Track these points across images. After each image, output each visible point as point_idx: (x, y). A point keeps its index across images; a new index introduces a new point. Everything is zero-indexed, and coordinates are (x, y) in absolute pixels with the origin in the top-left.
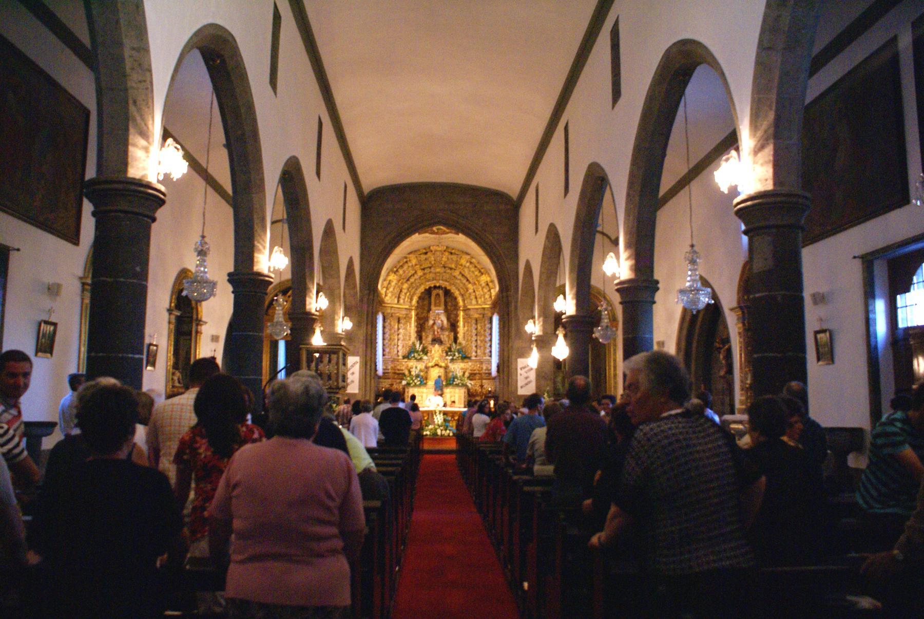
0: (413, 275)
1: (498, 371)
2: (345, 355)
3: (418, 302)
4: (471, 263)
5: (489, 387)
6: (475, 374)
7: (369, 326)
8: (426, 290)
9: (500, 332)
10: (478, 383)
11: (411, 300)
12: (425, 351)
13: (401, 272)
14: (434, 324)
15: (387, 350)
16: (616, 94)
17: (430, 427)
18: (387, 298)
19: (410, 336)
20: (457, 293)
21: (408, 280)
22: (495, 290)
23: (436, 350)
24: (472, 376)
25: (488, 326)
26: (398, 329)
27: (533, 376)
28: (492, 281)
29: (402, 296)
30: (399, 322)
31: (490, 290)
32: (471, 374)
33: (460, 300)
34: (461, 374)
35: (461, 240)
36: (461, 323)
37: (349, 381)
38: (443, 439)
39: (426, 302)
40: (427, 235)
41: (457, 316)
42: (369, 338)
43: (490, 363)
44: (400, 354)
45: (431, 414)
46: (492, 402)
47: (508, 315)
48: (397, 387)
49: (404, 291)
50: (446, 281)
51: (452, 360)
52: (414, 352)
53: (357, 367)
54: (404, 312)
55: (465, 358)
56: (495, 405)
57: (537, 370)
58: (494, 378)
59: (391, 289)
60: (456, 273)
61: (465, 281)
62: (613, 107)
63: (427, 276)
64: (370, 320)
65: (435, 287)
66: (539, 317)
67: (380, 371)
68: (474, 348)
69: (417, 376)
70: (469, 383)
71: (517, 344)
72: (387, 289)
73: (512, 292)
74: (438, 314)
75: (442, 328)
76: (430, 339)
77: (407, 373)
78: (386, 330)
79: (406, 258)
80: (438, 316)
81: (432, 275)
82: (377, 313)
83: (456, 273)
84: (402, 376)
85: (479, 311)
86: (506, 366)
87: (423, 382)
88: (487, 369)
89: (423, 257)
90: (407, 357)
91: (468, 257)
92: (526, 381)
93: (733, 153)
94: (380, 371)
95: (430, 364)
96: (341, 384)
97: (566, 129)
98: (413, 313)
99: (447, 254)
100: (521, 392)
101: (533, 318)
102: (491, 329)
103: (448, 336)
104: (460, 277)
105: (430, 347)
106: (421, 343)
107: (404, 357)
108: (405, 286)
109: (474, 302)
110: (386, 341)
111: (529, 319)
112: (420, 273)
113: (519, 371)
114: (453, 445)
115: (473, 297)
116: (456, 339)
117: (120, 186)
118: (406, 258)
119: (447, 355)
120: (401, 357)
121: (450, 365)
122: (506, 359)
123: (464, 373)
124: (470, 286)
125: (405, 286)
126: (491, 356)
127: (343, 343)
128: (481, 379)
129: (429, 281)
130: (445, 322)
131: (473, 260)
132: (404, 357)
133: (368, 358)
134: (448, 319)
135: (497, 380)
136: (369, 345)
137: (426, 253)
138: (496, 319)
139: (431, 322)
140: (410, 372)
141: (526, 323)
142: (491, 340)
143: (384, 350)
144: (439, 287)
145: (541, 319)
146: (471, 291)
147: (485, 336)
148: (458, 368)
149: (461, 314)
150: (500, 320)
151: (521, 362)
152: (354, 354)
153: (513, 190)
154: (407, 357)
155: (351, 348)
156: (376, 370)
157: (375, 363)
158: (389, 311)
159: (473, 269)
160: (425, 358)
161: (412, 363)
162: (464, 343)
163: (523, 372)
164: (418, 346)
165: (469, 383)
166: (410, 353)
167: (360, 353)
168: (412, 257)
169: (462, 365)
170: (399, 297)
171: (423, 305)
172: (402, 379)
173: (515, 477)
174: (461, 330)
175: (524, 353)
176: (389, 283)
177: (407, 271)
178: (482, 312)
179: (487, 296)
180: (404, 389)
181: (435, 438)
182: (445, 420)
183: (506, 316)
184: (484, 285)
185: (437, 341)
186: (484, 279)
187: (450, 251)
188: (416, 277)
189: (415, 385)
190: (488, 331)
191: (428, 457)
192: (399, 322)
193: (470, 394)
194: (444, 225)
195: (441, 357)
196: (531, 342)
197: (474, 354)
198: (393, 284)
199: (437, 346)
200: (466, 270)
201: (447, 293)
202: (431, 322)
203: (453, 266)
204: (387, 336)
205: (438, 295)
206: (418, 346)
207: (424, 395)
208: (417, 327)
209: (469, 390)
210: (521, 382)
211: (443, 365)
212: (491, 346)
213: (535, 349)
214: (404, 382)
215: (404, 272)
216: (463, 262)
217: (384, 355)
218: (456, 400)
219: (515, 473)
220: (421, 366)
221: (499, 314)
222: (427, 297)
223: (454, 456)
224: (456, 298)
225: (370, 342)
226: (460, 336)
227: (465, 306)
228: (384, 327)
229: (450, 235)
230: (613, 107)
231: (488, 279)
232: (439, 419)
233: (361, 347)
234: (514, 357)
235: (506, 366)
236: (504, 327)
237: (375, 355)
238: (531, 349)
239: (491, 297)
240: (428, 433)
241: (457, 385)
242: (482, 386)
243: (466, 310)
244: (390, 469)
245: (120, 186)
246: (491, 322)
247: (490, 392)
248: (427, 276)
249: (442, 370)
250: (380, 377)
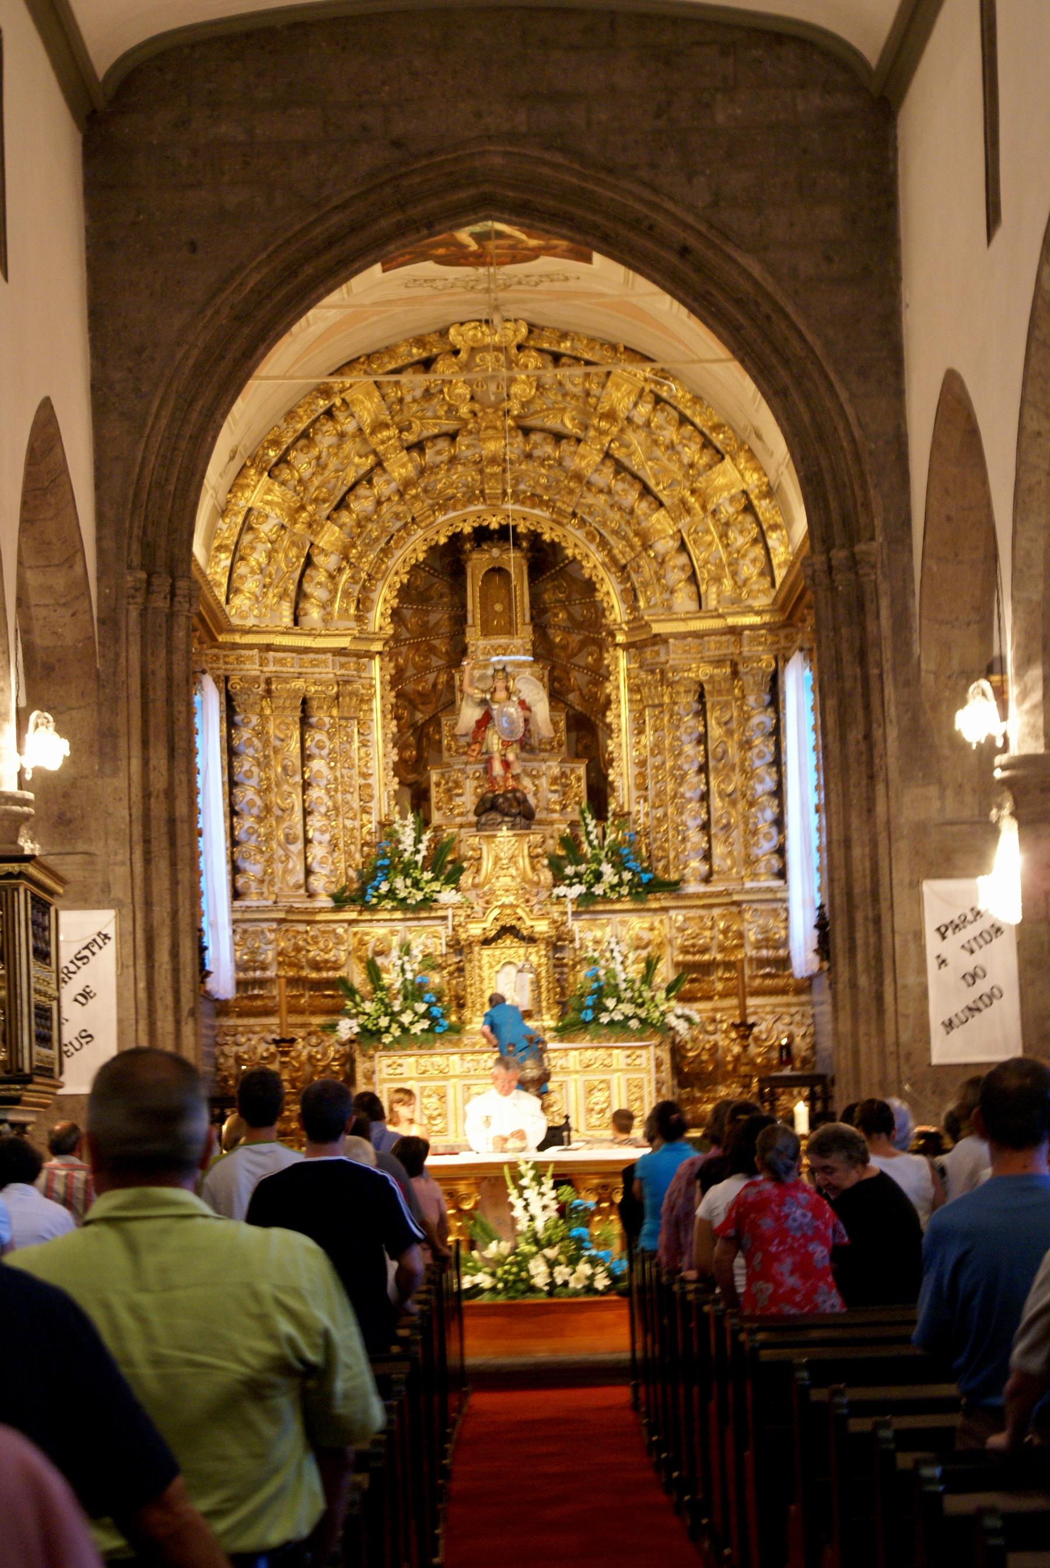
0: (367, 478)
1: (824, 947)
2: (41, 906)
3: (396, 615)
5: (777, 1024)
6: (707, 968)
7: (159, 756)
8: (433, 549)
9: (825, 750)
10: (727, 1011)
11: (363, 604)
12: (445, 863)
13: (303, 463)
14: (486, 721)
15: (253, 869)
17: (493, 1249)
18: (239, 601)
19: (366, 797)
20: (593, 562)
21: (342, 504)
22: (793, 529)
23: (504, 860)
24: (692, 979)
25: (763, 719)
26: (306, 757)
27: (1002, 963)
28: (770, 492)
29: (317, 591)
30: (305, 723)
31: (761, 538)
32: (684, 969)
33: (610, 591)
34: (635, 971)
35: (604, 290)
36: (621, 715)
37: (69, 1033)
38: (559, 1306)
39: (439, 616)
40: (428, 268)
41: (600, 675)
42: (158, 808)
43: (778, 906)
44: (318, 883)
45: (493, 1181)
46: (801, 1111)
47: (862, 657)
48: (316, 1050)
49: (326, 562)
50: (535, 500)
51: (587, 900)
52: (388, 871)
53: (107, 958)
54: (329, 670)
55: (651, 886)
56: (814, 1121)
57: (1020, 927)
58: (805, 986)
59: (257, 557)
60: (587, 459)
61: (630, 497)
63: (441, 481)
64: (158, 720)
65: (482, 535)
66: (1024, 664)
67: (223, 982)
68: (696, 838)
69: (414, 992)
70: (677, 1015)
71: (913, 805)
72: (238, 555)
73: (874, 548)
74: (503, 671)
75: (526, 744)
76: (467, 800)
77: (358, 978)
78: (245, 765)
79: (325, 392)
80: (505, 681)
81: (463, 475)
82: (192, 680)
83: (587, 459)
84: (332, 994)
85: (712, 648)
86: (861, 923)
87: (442, 1027)
88: (767, 942)
89: (414, 382)
90: (354, 897)
91: (646, 371)
92: (970, 996)
93: (883, 1136)
94: (223, 982)
95: (475, 930)
96: (31, 1054)
98: (376, 671)
99: (532, 360)
100: (947, 1049)
101: (992, 668)
102: (777, 733)
103: (561, 781)
104: (605, 477)
105: (470, 841)
106: (424, 823)
107: (340, 901)
108: (330, 536)
109: (683, 600)
110: (247, 822)
111: (970, 677)
112: (401, 467)
113: (933, 945)
114: (611, 1338)
115: (676, 576)
116: (599, 795)
118: (325, 392)
119: (559, 878)
120: (324, 901)
121: (575, 926)
122: (861, 886)
123: (651, 965)
124: (659, 521)
125: (330, 536)
126: (782, 874)
127: (28, 847)
128: (741, 992)
129: (445, 503)
130: (542, 709)
131: (671, 389)
132: (340, 901)
133: (161, 912)
134: (556, 697)
135: (822, 995)
136: (161, 844)
138: (798, 684)
139: (469, 715)
140: (374, 972)
141: (961, 701)
142: (779, 793)
143: (235, 870)
144: (504, 534)
145: (1036, 673)
146: (665, 545)
147: (749, 774)
148: (618, 939)
149: (621, 664)
150: (822, 689)
151: (940, 899)
152: (85, 901)
154: (354, 897)
155: (69, 867)
156: (203, 973)
157: (198, 933)
158: (252, 669)
159: (670, 434)
160: (448, 896)
161: (382, 929)
162: (640, 810)
163: (951, 946)
164: (407, 838)
165: (677, 1015)
166: (368, 878)
167: (120, 891)
168: (357, 382)
169: (637, 925)
170: (301, 595)
171: (425, 630)
172: (339, 1011)
173: (957, 1504)
174: (625, 747)
175: (960, 850)
176: (247, 527)
177: (335, 459)
178: (728, 648)
179: (749, 570)
180: (348, 1060)
181: (522, 1304)
182: (563, 1211)
183: (851, 669)
184: (728, 510)
185: (503, 807)
186: (729, 479)
187: (549, 346)
188: (382, 486)
189: (406, 1039)
190: (763, 747)
191: (482, 1401)
192: (305, 723)
193: (686, 1070)
194: (522, 212)
195: (527, 888)
196: (987, 791)
197: (696, 864)
198: (266, 529)
199: (504, 833)
200: (635, 439)
201: (544, 559)
202: (469, 715)
203: (569, 426)
204: (247, 794)
205: (498, 571)
206: (407, 838)
207: (453, 1089)
208: (398, 742)
209: (677, 1051)
210: (944, 996)
211: (542, 927)
212: (779, 822)
213: (1009, 830)
214: (347, 1027)
215: (320, 466)
216: (619, 397)
217: (236, 894)
218: (607, 1087)
219: (955, 1484)
220: (428, 938)
221: (808, 654)
222: (440, 586)
223: (620, 1394)
224: (590, 587)
225: (167, 834)
226: (622, 776)
227: (637, 623)
228: (231, 752)
229: (545, 264)
231: (752, 479)
232: (535, 1207)
233: (117, 859)
234: (901, 873)
235: (861, 923)
236: (843, 724)
237: (196, 895)
238: (994, 830)
239: (768, 570)
240: (484, 1280)
241: (619, 1027)
242: (744, 1028)
243: (644, 643)
246: (775, 701)
247: (786, 1051)
248: (441, 481)
249: (537, 955)
250: (222, 1008)
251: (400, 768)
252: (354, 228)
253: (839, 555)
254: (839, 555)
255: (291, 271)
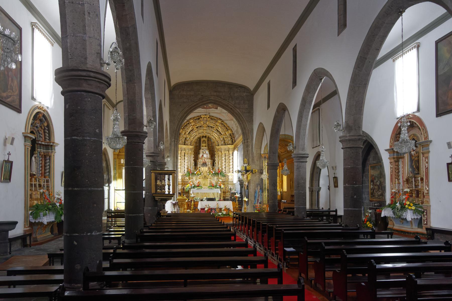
4: (45, 173)
16: (269, 106)
62: (338, 35)
65: (203, 137)
80: (205, 155)
97: (295, 50)
117: (84, 73)
137: (199, 119)
144: (206, 137)
153: (252, 87)
201: (209, 139)
230: (338, 35)
244: (146, 272)
245: (84, 73)
251: (194, 160)
252: (197, 104)
253: (246, 141)
254: (246, 141)
255: (191, 108)
